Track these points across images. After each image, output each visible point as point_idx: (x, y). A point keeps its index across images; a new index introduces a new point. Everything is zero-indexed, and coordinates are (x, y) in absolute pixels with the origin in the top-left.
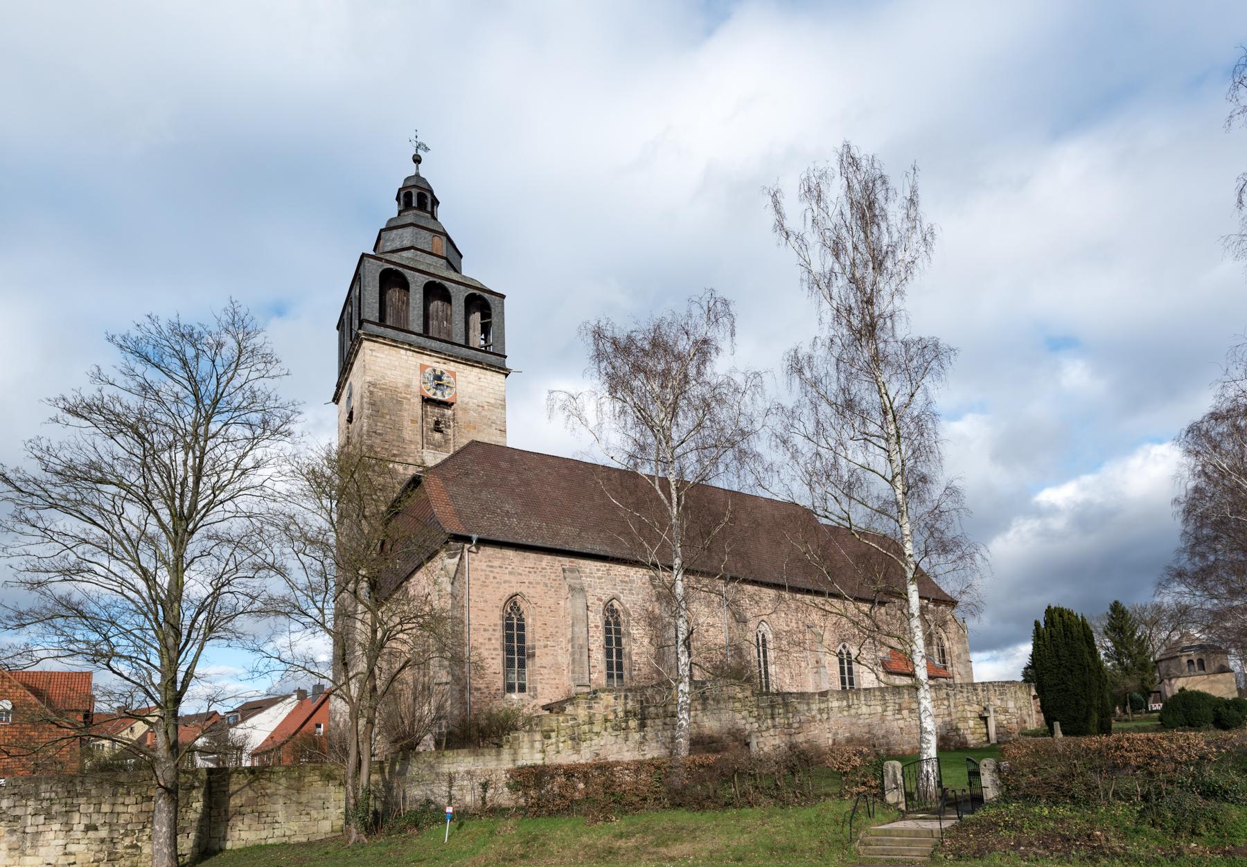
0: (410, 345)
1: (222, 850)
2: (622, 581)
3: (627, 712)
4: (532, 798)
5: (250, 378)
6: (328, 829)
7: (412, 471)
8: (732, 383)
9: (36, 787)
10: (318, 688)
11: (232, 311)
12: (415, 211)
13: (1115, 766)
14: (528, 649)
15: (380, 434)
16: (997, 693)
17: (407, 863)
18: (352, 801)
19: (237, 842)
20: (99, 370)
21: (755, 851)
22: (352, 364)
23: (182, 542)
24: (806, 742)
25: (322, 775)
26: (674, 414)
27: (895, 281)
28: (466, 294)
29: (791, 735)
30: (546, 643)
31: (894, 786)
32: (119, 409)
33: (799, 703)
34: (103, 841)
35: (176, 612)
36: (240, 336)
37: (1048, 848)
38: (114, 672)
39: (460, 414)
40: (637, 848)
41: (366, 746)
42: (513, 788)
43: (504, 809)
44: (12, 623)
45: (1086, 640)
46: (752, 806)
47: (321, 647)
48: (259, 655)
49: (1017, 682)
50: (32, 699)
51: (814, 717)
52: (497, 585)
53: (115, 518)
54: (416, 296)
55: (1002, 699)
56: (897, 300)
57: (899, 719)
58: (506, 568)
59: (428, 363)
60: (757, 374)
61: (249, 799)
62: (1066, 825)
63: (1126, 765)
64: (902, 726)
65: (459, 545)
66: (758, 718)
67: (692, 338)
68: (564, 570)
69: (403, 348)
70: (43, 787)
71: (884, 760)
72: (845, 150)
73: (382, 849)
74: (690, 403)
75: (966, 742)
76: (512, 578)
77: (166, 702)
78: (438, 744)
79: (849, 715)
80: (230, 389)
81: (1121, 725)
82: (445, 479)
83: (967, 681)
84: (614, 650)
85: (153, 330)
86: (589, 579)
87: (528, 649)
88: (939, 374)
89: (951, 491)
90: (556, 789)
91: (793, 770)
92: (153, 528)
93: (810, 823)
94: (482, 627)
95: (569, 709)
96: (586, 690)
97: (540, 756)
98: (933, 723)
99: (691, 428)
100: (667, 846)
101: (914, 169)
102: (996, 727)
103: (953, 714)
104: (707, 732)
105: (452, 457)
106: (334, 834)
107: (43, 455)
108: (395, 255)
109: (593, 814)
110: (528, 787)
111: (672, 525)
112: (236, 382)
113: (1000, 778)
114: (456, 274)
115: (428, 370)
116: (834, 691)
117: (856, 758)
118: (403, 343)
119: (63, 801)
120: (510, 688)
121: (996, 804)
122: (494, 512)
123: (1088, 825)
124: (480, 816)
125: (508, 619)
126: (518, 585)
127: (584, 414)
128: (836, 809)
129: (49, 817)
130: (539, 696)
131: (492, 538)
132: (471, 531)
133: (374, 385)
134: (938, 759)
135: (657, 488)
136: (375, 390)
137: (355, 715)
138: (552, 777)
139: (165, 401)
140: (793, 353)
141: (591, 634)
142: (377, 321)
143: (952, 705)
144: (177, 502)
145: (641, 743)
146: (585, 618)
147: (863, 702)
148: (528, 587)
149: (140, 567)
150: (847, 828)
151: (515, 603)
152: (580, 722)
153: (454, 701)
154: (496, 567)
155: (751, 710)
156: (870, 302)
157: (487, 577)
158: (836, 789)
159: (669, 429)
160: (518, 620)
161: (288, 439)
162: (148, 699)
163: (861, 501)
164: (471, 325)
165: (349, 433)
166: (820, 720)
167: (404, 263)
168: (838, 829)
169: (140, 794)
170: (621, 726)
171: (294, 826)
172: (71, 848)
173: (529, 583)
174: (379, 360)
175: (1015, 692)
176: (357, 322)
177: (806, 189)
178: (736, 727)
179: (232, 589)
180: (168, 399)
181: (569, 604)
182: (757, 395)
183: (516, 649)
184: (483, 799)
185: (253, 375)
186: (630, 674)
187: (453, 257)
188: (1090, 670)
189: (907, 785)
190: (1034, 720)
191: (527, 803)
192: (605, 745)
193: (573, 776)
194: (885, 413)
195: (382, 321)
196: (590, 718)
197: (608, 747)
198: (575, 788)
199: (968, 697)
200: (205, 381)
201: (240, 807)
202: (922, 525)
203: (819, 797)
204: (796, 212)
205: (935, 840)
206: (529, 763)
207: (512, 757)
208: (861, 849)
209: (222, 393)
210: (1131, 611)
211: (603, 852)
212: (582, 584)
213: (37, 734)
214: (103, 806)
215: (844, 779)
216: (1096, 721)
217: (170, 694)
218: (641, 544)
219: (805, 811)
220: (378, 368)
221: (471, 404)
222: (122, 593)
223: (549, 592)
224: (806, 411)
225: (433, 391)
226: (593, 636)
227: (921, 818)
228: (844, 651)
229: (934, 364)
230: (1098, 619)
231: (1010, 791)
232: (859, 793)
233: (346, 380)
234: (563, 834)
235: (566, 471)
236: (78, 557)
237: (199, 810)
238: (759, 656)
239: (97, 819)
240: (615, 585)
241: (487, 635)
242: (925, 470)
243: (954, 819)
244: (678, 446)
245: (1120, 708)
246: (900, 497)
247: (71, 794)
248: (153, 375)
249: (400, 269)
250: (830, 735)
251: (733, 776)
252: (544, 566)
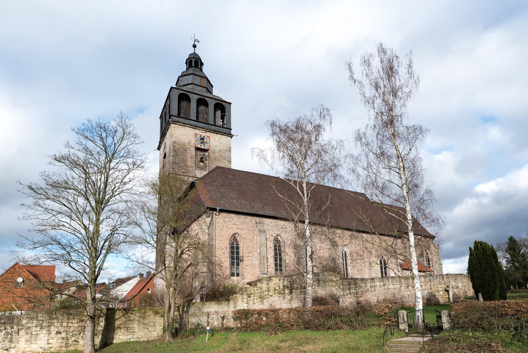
0: (191, 125)
1: (112, 343)
2: (282, 228)
3: (284, 286)
4: (243, 324)
5: (128, 144)
6: (156, 335)
7: (191, 180)
8: (330, 144)
9: (37, 315)
10: (149, 273)
11: (121, 117)
12: (193, 68)
13: (502, 314)
14: (241, 257)
15: (178, 164)
16: (453, 279)
17: (190, 351)
18: (167, 324)
19: (118, 340)
20: (68, 143)
21: (341, 349)
22: (166, 134)
23: (99, 213)
24: (365, 301)
25: (153, 312)
26: (305, 158)
27: (403, 100)
28: (215, 103)
29: (358, 297)
30: (248, 255)
31: (403, 322)
32: (76, 159)
33: (361, 283)
34: (63, 338)
35: (96, 242)
36: (124, 127)
37: (471, 350)
38: (72, 267)
39: (211, 154)
40: (289, 346)
41: (173, 300)
42: (235, 319)
43: (231, 328)
44: (31, 247)
45: (493, 256)
46: (340, 329)
47: (151, 256)
48: (129, 260)
49: (463, 274)
50: (31, 277)
51: (368, 289)
52: (227, 230)
53: (74, 204)
54: (193, 104)
55: (456, 282)
56: (403, 109)
57: (407, 291)
58: (231, 222)
59: (198, 133)
60: (341, 141)
61: (123, 322)
62: (479, 340)
63: (507, 314)
64: (409, 294)
65: (211, 212)
66: (343, 290)
67: (313, 125)
68: (256, 223)
69: (188, 127)
70: (40, 315)
71: (399, 310)
72: (380, 46)
73: (179, 344)
74: (312, 152)
75: (439, 301)
76: (234, 226)
77: (92, 280)
78: (202, 299)
79: (385, 289)
80: (119, 149)
81: (512, 294)
82: (205, 183)
83: (440, 273)
84: (278, 258)
85: (89, 126)
86: (267, 227)
87: (241, 257)
88: (422, 140)
89: (428, 192)
90: (254, 320)
91: (358, 314)
92: (88, 208)
93: (365, 337)
94: (221, 248)
95: (259, 284)
96: (266, 276)
97: (246, 305)
98: (421, 294)
99: (313, 163)
100: (302, 346)
101: (411, 52)
102: (453, 295)
103: (433, 289)
104: (320, 295)
105: (208, 173)
106: (158, 338)
107: (46, 177)
108: (185, 87)
109: (270, 331)
110: (241, 319)
111: (304, 206)
112: (122, 146)
113: (450, 319)
114: (210, 94)
115: (198, 136)
116: (377, 278)
117: (386, 309)
118: (188, 124)
119: (48, 321)
120: (233, 275)
121: (448, 331)
122: (226, 198)
123: (489, 341)
124: (221, 331)
125: (232, 244)
126: (237, 229)
127: (266, 158)
128: (377, 331)
129: (42, 328)
130: (245, 278)
131: (225, 209)
132: (216, 206)
133: (175, 143)
134: (423, 310)
135: (298, 189)
136: (176, 145)
137: (168, 286)
138: (252, 315)
139: (93, 154)
140: (357, 132)
141: (268, 251)
142: (177, 115)
143: (432, 285)
144: (97, 196)
145: (290, 300)
146: (265, 244)
147: (391, 283)
148: (241, 230)
149: (83, 224)
150: (382, 339)
151: (235, 237)
152: (264, 290)
153: (209, 280)
154: (227, 222)
155: (339, 286)
156: (391, 110)
157: (223, 226)
158: (377, 322)
159: (303, 164)
160: (236, 245)
161: (143, 170)
162: (85, 279)
163: (388, 195)
164: (217, 116)
165: (164, 163)
166: (371, 291)
167: (188, 90)
168: (378, 340)
169: (79, 319)
170: (281, 292)
171: (142, 334)
172: (50, 341)
173: (242, 228)
174: (178, 132)
175: (462, 279)
176: (168, 116)
177: (363, 61)
178: (333, 293)
179: (118, 232)
180: (95, 153)
181: (258, 238)
182: (342, 150)
183: (235, 258)
184: (222, 323)
185: (129, 144)
186: (285, 269)
187: (209, 87)
188: (495, 270)
189: (409, 321)
190: (471, 292)
191: (241, 326)
192: (275, 301)
193: (261, 314)
194: (398, 157)
195: (179, 116)
196: (268, 288)
197: (276, 301)
198: (262, 319)
199: (440, 281)
200: (110, 146)
201: (120, 325)
202: (415, 207)
203: (370, 326)
204: (359, 71)
205: (421, 346)
206: (242, 308)
207: (234, 305)
208: (388, 349)
209: (116, 150)
210: (518, 241)
211: (275, 348)
212: (264, 229)
213: (32, 292)
214: (63, 323)
215: (381, 318)
216: (498, 293)
217: (93, 277)
218: (291, 214)
219: (363, 332)
221: (216, 150)
222: (74, 234)
223: (250, 233)
224: (363, 158)
225: (200, 145)
226: (269, 252)
227: (415, 336)
228: (382, 259)
229: (420, 136)
230: (503, 244)
231: (455, 325)
232: (387, 325)
233: (163, 140)
234: (257, 340)
235: (257, 179)
236: (58, 220)
237: (103, 326)
238: (343, 261)
239: (61, 329)
240: (279, 229)
241: (223, 251)
242: (416, 182)
243: (430, 337)
244: (307, 171)
245: (513, 287)
246: (405, 194)
247: (51, 318)
248: (90, 145)
249: (187, 93)
250: (375, 298)
251: (331, 316)
252: (248, 221)
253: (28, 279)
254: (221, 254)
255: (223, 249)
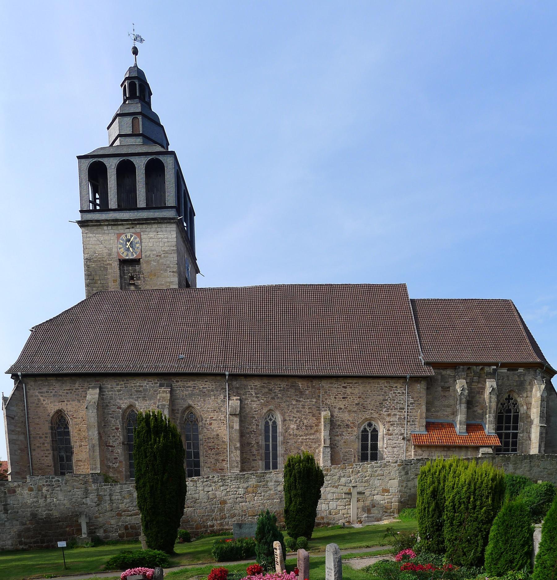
2: (136, 391)
58: (51, 392)
220: (91, 246)
254: (39, 445)
255: (42, 438)
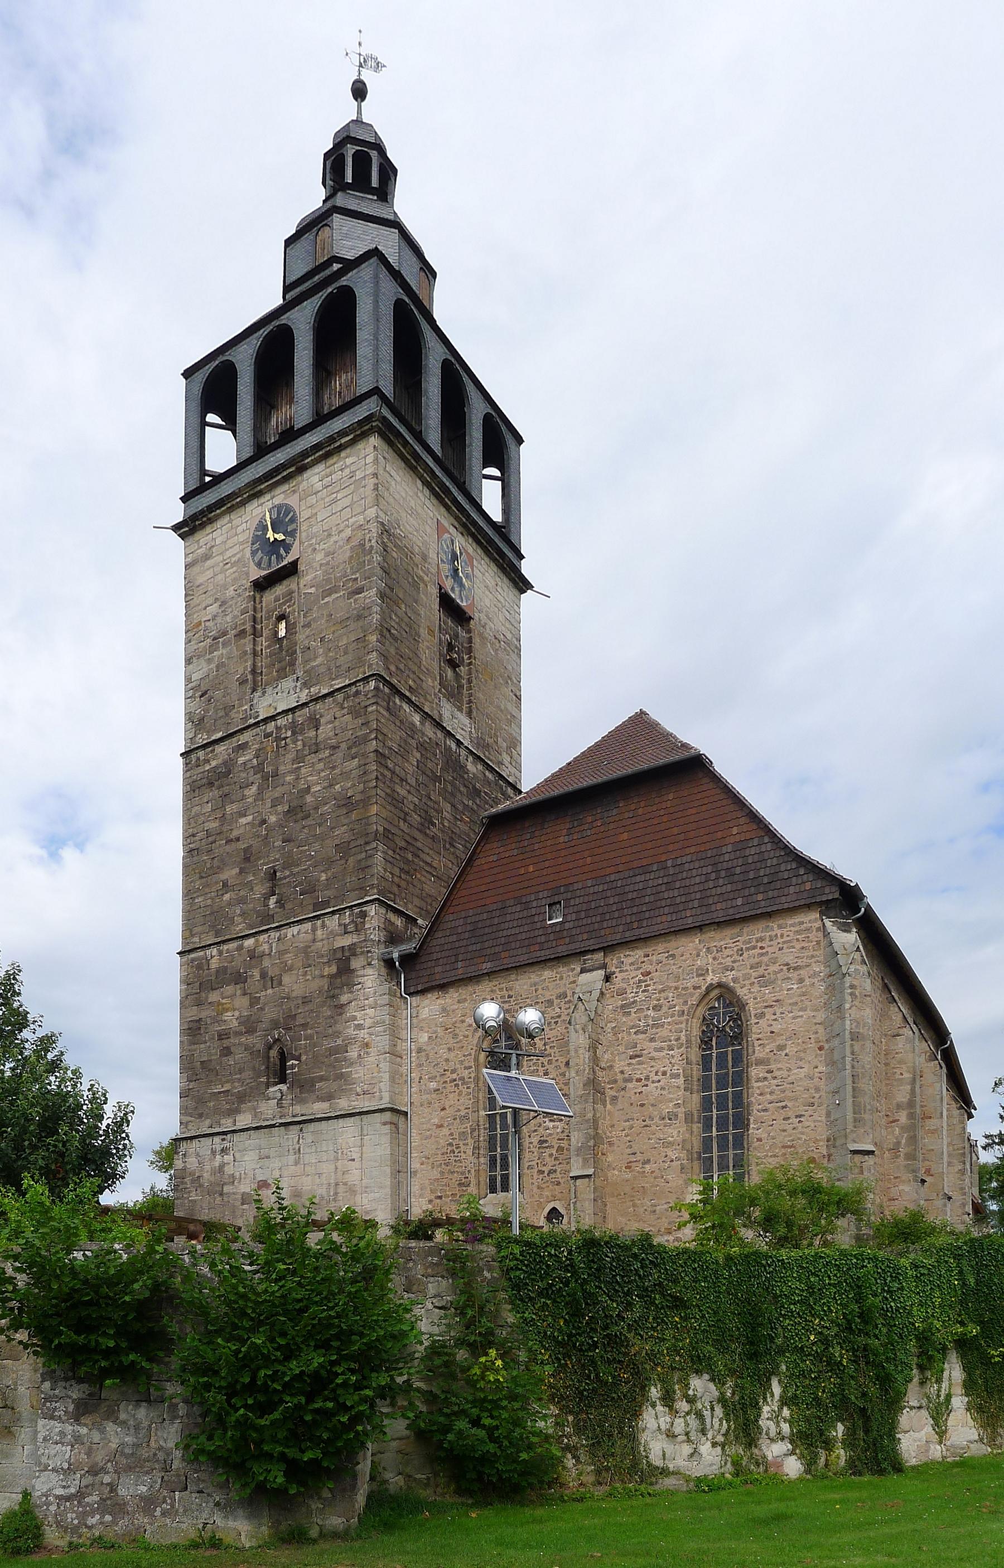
253: (468, 1306)
